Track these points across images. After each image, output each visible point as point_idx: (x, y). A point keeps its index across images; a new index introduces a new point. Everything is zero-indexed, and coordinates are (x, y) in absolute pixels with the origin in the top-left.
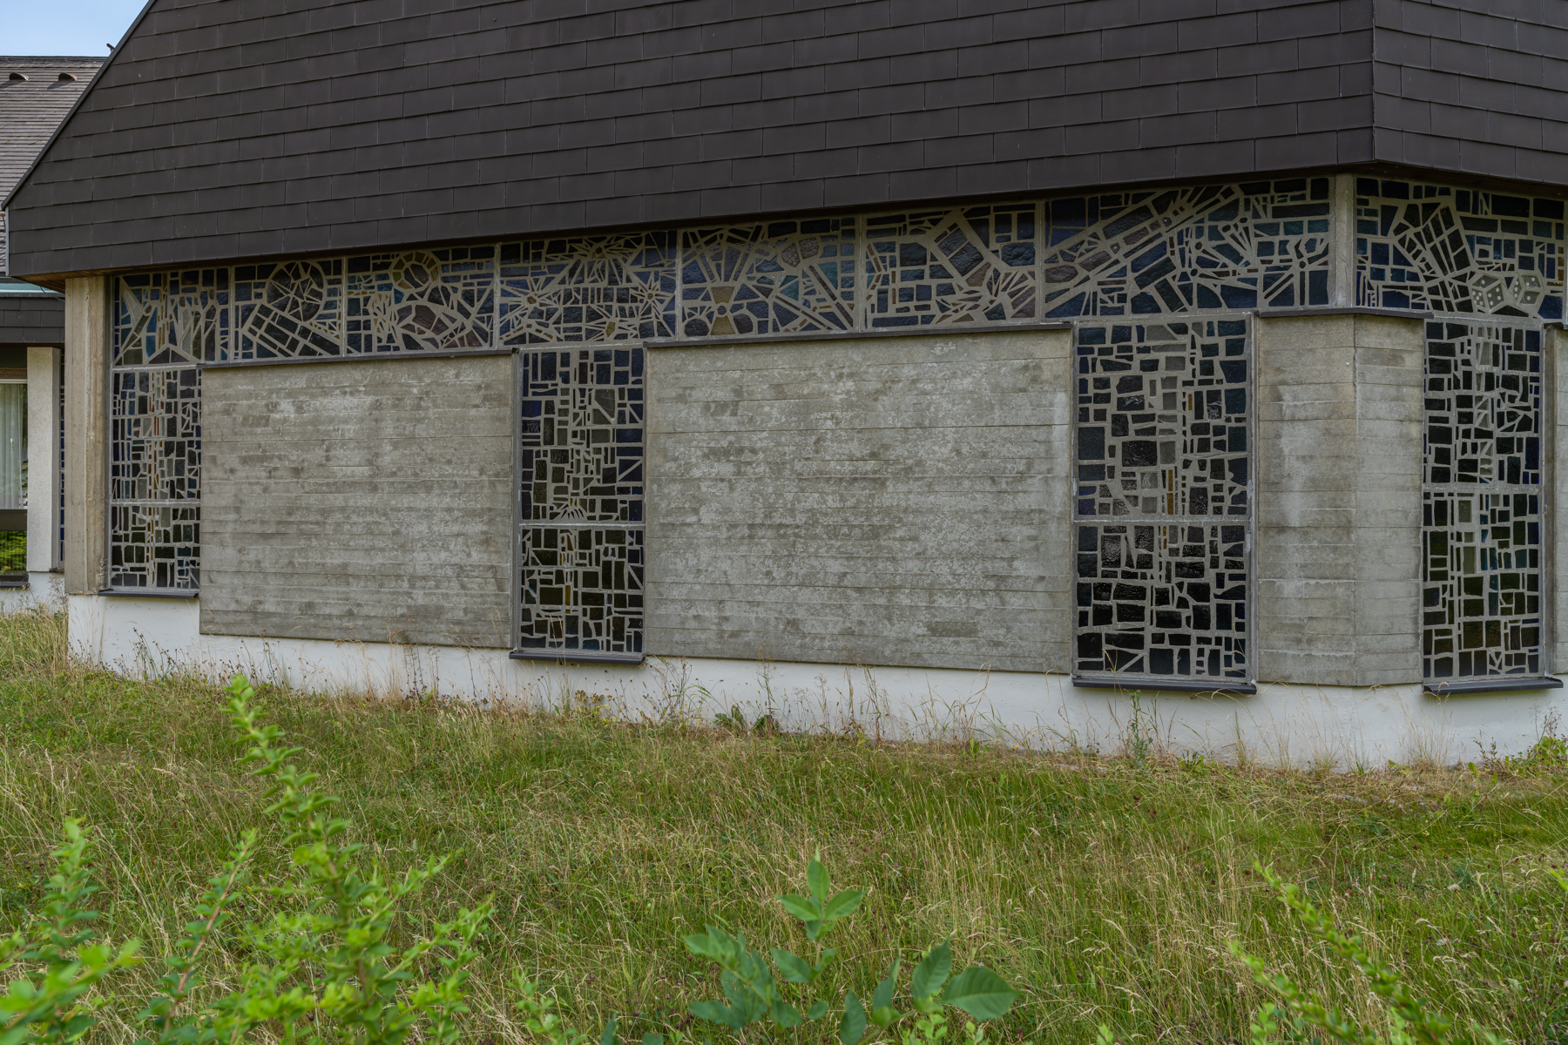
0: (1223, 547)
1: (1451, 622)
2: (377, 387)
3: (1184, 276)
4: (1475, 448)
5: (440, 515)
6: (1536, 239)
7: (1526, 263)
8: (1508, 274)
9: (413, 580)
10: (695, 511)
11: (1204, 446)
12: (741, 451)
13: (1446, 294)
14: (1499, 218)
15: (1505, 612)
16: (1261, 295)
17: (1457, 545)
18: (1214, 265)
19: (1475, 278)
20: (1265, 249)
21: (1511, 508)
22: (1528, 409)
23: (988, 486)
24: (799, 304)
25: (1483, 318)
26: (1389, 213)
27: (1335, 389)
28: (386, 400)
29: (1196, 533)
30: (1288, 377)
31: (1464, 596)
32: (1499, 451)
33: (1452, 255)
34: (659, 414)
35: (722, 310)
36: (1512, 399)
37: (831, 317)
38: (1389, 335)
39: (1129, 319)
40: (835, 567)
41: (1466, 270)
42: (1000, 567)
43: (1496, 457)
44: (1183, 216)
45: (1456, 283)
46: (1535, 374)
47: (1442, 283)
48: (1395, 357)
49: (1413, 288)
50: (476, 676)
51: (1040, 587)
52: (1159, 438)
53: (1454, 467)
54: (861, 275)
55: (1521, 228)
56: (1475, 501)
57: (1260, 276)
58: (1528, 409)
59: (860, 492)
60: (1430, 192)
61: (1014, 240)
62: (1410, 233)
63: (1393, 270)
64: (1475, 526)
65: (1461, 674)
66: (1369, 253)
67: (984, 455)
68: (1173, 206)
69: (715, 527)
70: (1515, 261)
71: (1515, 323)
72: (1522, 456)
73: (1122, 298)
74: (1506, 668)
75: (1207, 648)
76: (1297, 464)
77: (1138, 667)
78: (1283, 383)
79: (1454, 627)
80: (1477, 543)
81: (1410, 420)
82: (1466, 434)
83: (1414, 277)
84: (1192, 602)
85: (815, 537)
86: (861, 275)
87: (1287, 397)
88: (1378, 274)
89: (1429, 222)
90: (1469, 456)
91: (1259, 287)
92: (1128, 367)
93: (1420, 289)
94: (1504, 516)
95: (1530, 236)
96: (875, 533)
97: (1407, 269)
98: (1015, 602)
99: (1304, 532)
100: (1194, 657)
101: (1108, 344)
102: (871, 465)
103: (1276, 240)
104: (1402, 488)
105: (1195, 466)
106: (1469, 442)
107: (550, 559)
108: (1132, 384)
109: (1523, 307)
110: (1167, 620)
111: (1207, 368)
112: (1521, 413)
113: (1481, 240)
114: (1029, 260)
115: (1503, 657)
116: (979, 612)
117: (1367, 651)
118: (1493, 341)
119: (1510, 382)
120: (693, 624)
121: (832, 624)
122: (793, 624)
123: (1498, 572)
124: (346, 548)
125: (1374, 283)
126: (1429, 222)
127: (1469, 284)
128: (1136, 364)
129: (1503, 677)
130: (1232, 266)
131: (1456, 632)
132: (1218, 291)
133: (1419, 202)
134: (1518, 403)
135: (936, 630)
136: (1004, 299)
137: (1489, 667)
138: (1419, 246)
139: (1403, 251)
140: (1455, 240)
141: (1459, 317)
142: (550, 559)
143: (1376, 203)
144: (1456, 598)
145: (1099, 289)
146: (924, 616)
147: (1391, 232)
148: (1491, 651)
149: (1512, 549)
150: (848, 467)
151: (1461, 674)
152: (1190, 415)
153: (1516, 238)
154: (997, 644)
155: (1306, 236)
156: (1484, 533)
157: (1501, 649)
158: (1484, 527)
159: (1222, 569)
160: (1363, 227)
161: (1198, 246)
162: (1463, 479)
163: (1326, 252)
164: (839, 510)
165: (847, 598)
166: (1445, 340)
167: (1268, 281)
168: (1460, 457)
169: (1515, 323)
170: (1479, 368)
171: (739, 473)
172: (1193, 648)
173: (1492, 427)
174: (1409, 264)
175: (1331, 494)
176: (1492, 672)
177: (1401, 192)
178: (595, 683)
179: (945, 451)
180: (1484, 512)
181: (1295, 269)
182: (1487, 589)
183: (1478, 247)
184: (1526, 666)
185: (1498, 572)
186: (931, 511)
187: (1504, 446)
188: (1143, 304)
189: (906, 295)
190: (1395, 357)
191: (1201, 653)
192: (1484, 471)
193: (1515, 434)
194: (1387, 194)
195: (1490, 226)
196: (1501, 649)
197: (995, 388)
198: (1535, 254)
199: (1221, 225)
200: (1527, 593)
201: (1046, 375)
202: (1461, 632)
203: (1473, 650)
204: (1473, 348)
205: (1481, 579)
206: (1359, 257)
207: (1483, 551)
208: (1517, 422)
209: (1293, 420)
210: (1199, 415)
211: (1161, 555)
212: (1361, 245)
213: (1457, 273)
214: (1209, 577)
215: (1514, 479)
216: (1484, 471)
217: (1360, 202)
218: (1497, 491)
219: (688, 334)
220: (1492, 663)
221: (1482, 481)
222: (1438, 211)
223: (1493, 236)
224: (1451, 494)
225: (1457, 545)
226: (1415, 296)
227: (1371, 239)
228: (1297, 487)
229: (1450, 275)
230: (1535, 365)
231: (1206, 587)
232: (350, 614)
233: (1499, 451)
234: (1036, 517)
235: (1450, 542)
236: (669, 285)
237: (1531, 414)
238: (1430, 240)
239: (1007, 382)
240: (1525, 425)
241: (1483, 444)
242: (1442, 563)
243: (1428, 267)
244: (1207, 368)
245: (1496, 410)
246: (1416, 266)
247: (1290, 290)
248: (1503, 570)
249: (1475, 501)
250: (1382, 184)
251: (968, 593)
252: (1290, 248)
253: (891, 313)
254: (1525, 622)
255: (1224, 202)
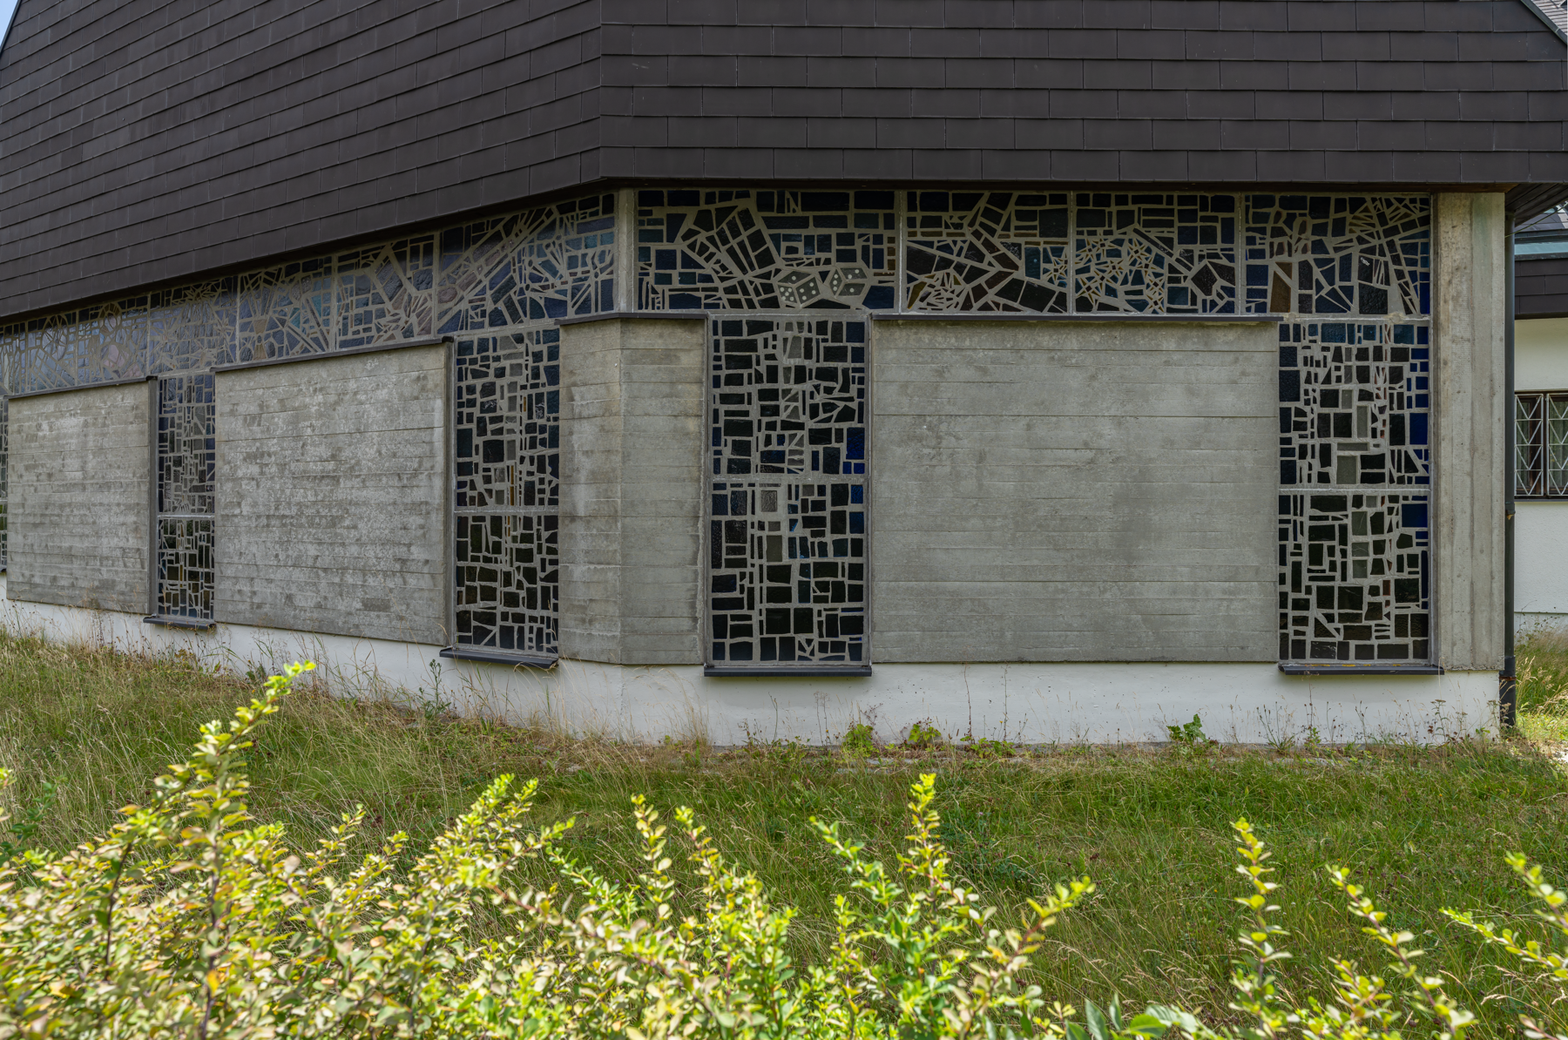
0: (545, 535)
1: (751, 607)
2: (86, 410)
3: (521, 292)
4: (781, 440)
5: (115, 509)
6: (857, 231)
7: (845, 256)
8: (823, 268)
9: (103, 559)
10: (239, 504)
11: (533, 446)
12: (262, 455)
13: (746, 292)
14: (810, 214)
15: (818, 600)
16: (570, 304)
17: (758, 533)
18: (539, 279)
19: (781, 275)
20: (572, 263)
21: (828, 498)
22: (851, 399)
23: (396, 482)
24: (299, 331)
25: (793, 311)
26: (675, 222)
27: (608, 389)
28: (90, 420)
29: (528, 522)
30: (577, 379)
31: (767, 584)
32: (812, 442)
33: (752, 255)
34: (224, 426)
35: (259, 339)
36: (829, 390)
37: (316, 340)
38: (661, 336)
39: (488, 332)
40: (312, 550)
41: (772, 268)
42: (401, 551)
43: (808, 449)
44: (522, 236)
45: (758, 281)
46: (858, 365)
47: (741, 283)
48: (669, 356)
49: (704, 289)
50: (130, 634)
51: (426, 570)
52: (506, 437)
53: (755, 459)
54: (334, 304)
55: (842, 222)
56: (782, 494)
57: (568, 287)
58: (851, 399)
59: (325, 487)
60: (725, 197)
61: (421, 268)
62: (702, 237)
63: (681, 274)
64: (782, 515)
65: (763, 658)
66: (653, 260)
67: (394, 455)
68: (515, 229)
69: (250, 518)
70: (832, 255)
71: (831, 316)
72: (843, 447)
73: (483, 314)
74: (818, 655)
75: (536, 626)
76: (583, 459)
77: (492, 642)
78: (575, 385)
79: (754, 614)
80: (785, 532)
81: (687, 416)
82: (771, 426)
83: (708, 279)
84: (526, 584)
85: (301, 526)
86: (334, 304)
87: (577, 397)
88: (665, 279)
89: (724, 226)
90: (774, 447)
91: (568, 298)
92: (486, 374)
93: (716, 289)
94: (819, 506)
95: (851, 229)
96: (334, 522)
97: (698, 271)
98: (412, 581)
99: (588, 520)
100: (527, 635)
101: (475, 355)
102: (331, 466)
103: (579, 253)
104: (677, 480)
105: (527, 461)
106: (774, 434)
107: (172, 545)
108: (489, 390)
109: (843, 300)
110: (511, 600)
111: (536, 375)
112: (841, 404)
113: (787, 238)
114: (429, 285)
115: (815, 644)
116: (391, 590)
117: (634, 632)
118: (805, 334)
119: (824, 374)
120: (237, 597)
121: (306, 600)
122: (289, 597)
123: (811, 560)
124: (72, 535)
125: (659, 288)
126: (724, 226)
127: (774, 281)
128: (491, 372)
129: (816, 662)
130: (551, 280)
131: (757, 618)
132: (542, 303)
133: (712, 207)
134: (836, 394)
135: (369, 606)
136: (414, 319)
137: (798, 653)
138: (712, 249)
139: (694, 256)
140: (757, 240)
141: (761, 314)
142: (172, 545)
143: (659, 213)
144: (756, 585)
145: (469, 306)
146: (360, 594)
147: (679, 238)
148: (801, 638)
149: (829, 538)
150: (319, 467)
151: (763, 658)
152: (525, 415)
153: (833, 232)
154: (401, 618)
155: (599, 248)
156: (793, 523)
157: (815, 636)
158: (793, 516)
159: (544, 555)
160: (644, 236)
161: (530, 263)
162: (766, 470)
163: (611, 264)
164: (314, 503)
165: (318, 576)
166: (745, 336)
167: (575, 290)
168: (762, 448)
169: (831, 316)
170: (785, 361)
171: (262, 473)
172: (527, 625)
173: (803, 419)
174: (701, 267)
175: (604, 486)
176: (801, 658)
177: (692, 200)
178: (181, 641)
179: (372, 452)
180: (793, 502)
181: (592, 280)
182: (796, 577)
183: (784, 245)
184: (847, 654)
185: (811, 560)
186: (365, 504)
187: (818, 436)
188: (497, 319)
189: (359, 320)
190: (669, 356)
191: (531, 631)
192: (792, 462)
193: (834, 425)
194: (672, 203)
195: (803, 223)
196: (815, 636)
197: (401, 396)
198: (858, 245)
199: (545, 242)
200: (847, 582)
201: (430, 385)
202: (763, 618)
203: (777, 636)
204: (779, 343)
205: (788, 567)
206: (642, 264)
207: (792, 541)
208: (835, 413)
209: (581, 418)
210: (530, 417)
211: (507, 543)
212: (643, 254)
213: (759, 271)
214: (536, 564)
215: (831, 468)
216: (792, 462)
217: (641, 213)
218: (810, 481)
219: (1078, 310)
220: (802, 648)
221: (790, 471)
222: (734, 214)
223: (804, 232)
224: (752, 485)
225: (758, 533)
226: (707, 297)
227: (654, 247)
228: (583, 479)
229: (750, 275)
230: (859, 355)
231: (534, 570)
232: (73, 585)
233: (812, 442)
234: (423, 507)
235: (750, 531)
236: (233, 322)
237: (854, 405)
238: (725, 241)
239: (407, 392)
240: (846, 415)
241: (792, 437)
242: (742, 550)
243: (724, 268)
244: (536, 375)
245: (809, 401)
246: (708, 268)
247: (588, 299)
248: (817, 559)
249: (782, 494)
250: (665, 199)
251: (385, 573)
252: (588, 260)
253: (350, 336)
254: (844, 610)
255: (547, 222)
